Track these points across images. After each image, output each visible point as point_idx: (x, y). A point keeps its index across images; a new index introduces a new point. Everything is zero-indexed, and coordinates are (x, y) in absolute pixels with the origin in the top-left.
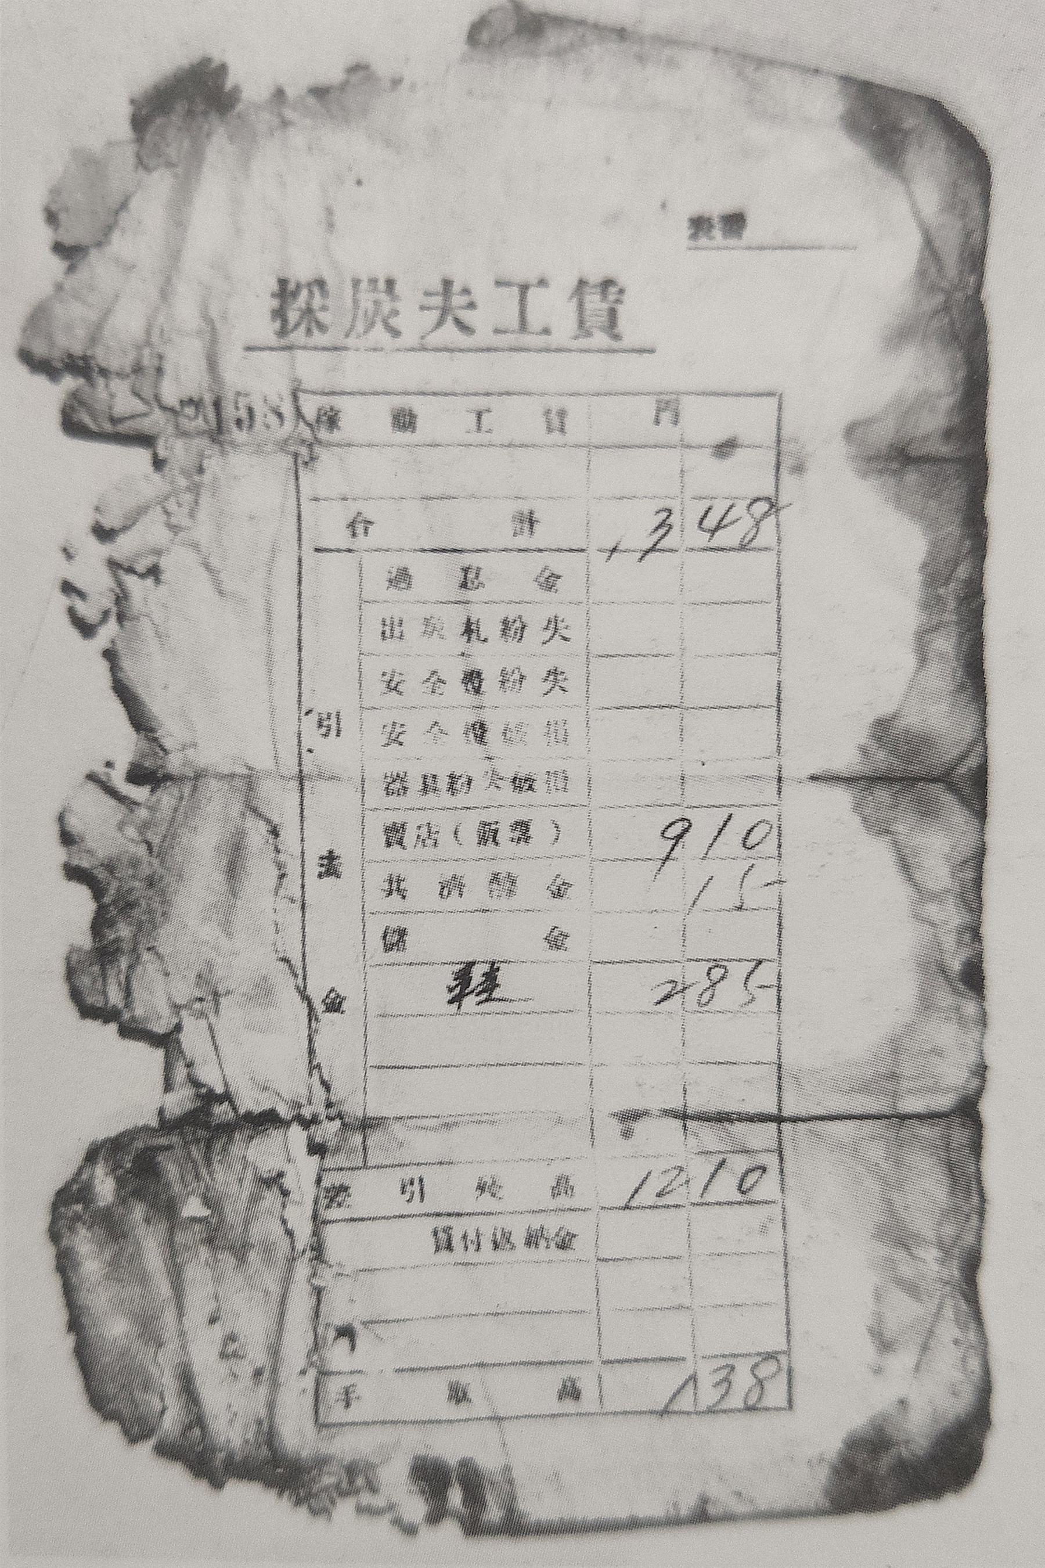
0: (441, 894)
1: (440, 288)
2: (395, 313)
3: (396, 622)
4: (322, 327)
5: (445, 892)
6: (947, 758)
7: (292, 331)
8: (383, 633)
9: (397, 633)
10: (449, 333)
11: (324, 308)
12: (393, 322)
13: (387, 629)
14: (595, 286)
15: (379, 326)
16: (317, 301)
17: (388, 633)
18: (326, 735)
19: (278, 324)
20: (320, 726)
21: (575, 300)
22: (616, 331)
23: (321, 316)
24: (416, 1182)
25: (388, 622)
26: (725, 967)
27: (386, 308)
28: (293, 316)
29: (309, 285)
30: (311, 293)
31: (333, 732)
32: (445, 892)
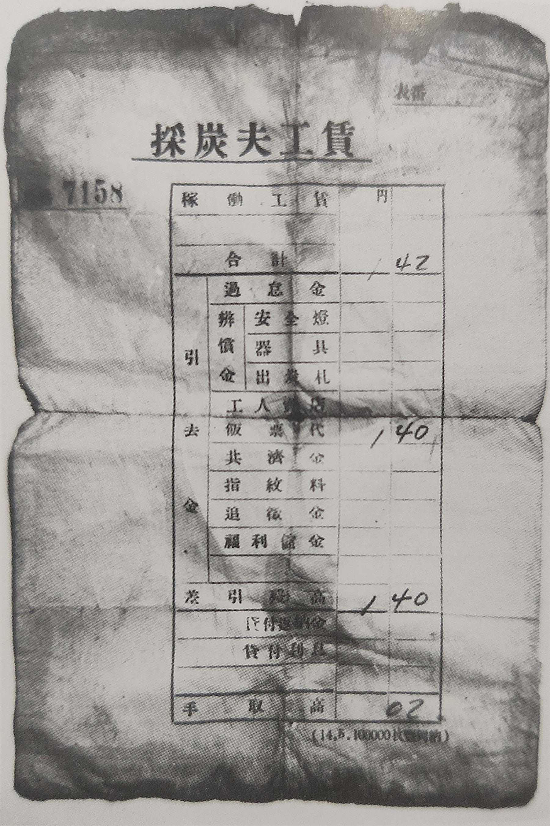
0: (269, 461)
1: (248, 128)
2: (223, 143)
3: (265, 373)
4: (182, 152)
5: (272, 460)
6: (541, 386)
7: (163, 153)
8: (258, 380)
9: (265, 380)
10: (254, 154)
11: (182, 141)
12: (222, 149)
13: (260, 378)
14: (337, 125)
15: (214, 151)
16: (178, 138)
17: (260, 380)
18: (190, 364)
19: (154, 149)
20: (187, 359)
21: (326, 133)
22: (350, 151)
23: (180, 145)
24: (237, 592)
25: (260, 373)
26: (427, 427)
27: (218, 141)
28: (164, 146)
29: (173, 129)
30: (175, 134)
31: (194, 362)
32: (272, 460)
